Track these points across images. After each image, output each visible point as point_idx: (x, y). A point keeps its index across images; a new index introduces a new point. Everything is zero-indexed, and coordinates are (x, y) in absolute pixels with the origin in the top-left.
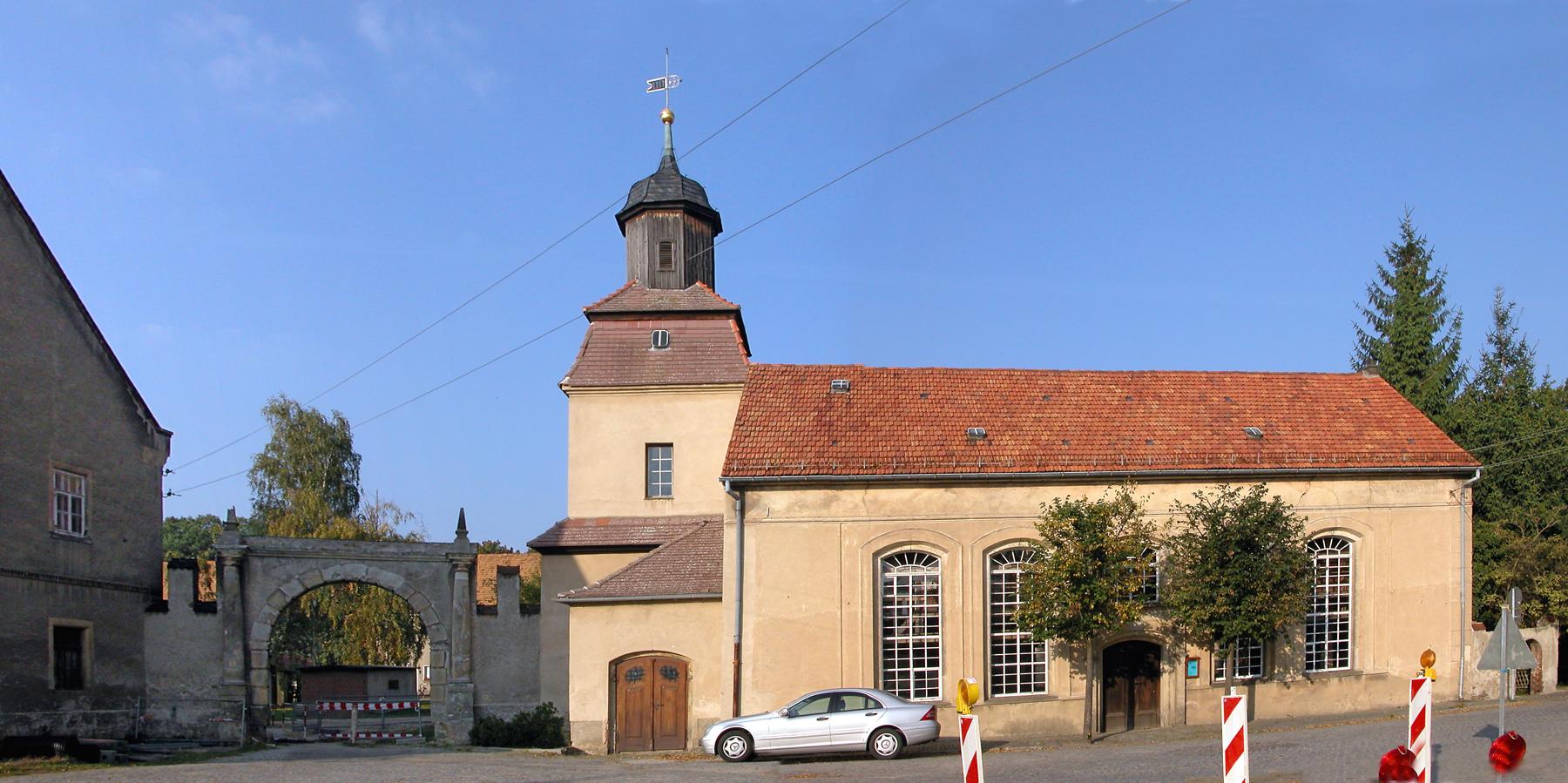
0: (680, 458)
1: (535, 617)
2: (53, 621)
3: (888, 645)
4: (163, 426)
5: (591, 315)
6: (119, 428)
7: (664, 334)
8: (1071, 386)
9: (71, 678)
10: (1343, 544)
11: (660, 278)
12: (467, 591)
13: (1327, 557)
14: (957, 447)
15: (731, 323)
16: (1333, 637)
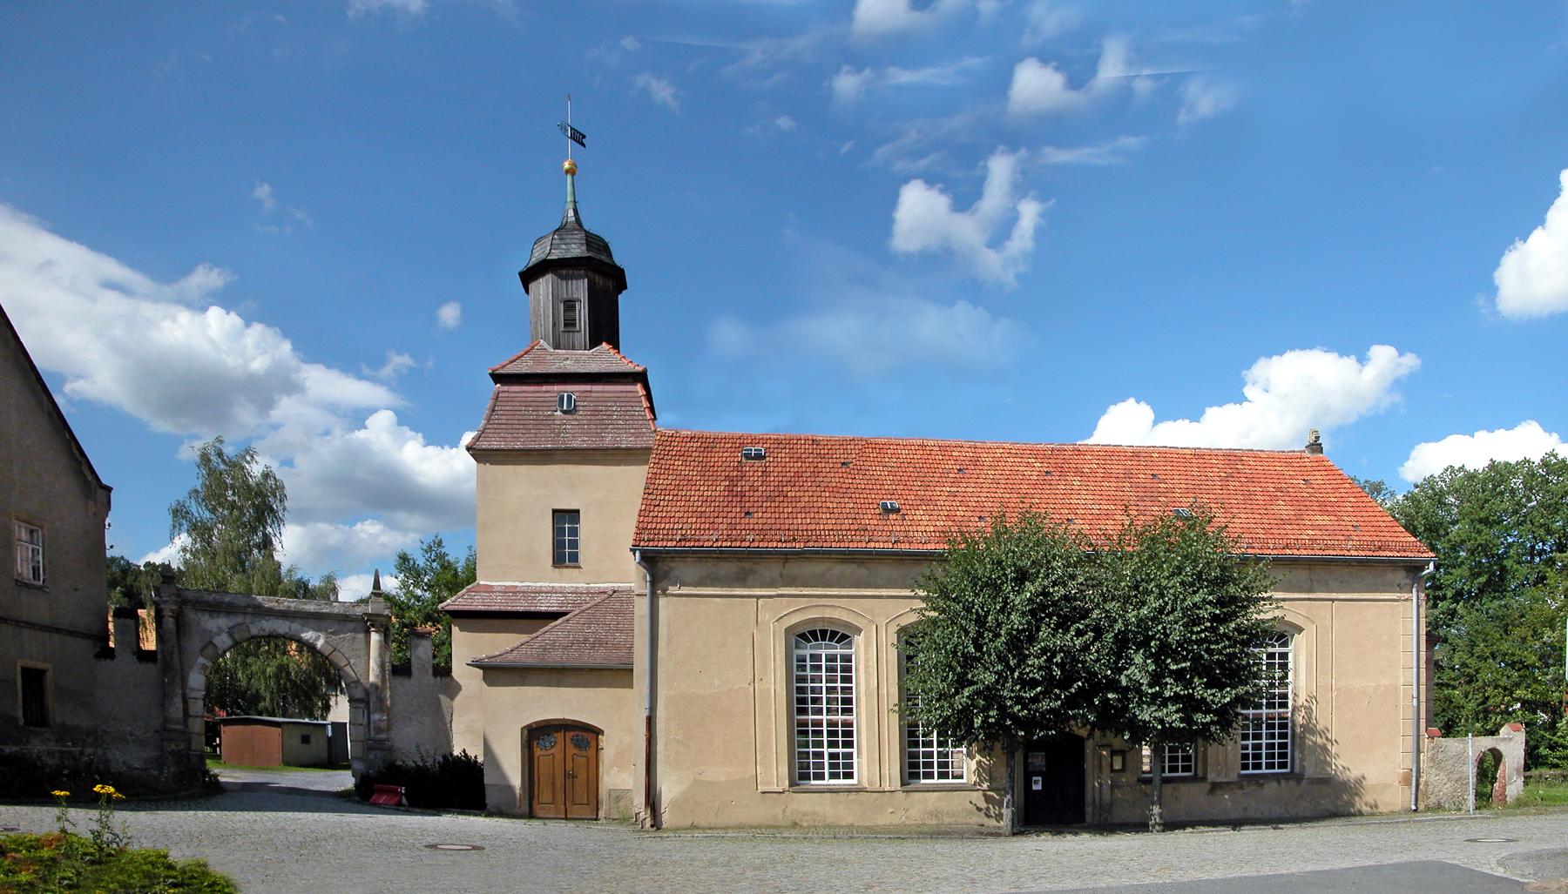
0: (585, 526)
2: (20, 663)
4: (104, 482)
5: (497, 378)
6: (65, 483)
7: (569, 398)
8: (987, 459)
9: (37, 716)
11: (563, 338)
14: (871, 521)
15: (639, 387)
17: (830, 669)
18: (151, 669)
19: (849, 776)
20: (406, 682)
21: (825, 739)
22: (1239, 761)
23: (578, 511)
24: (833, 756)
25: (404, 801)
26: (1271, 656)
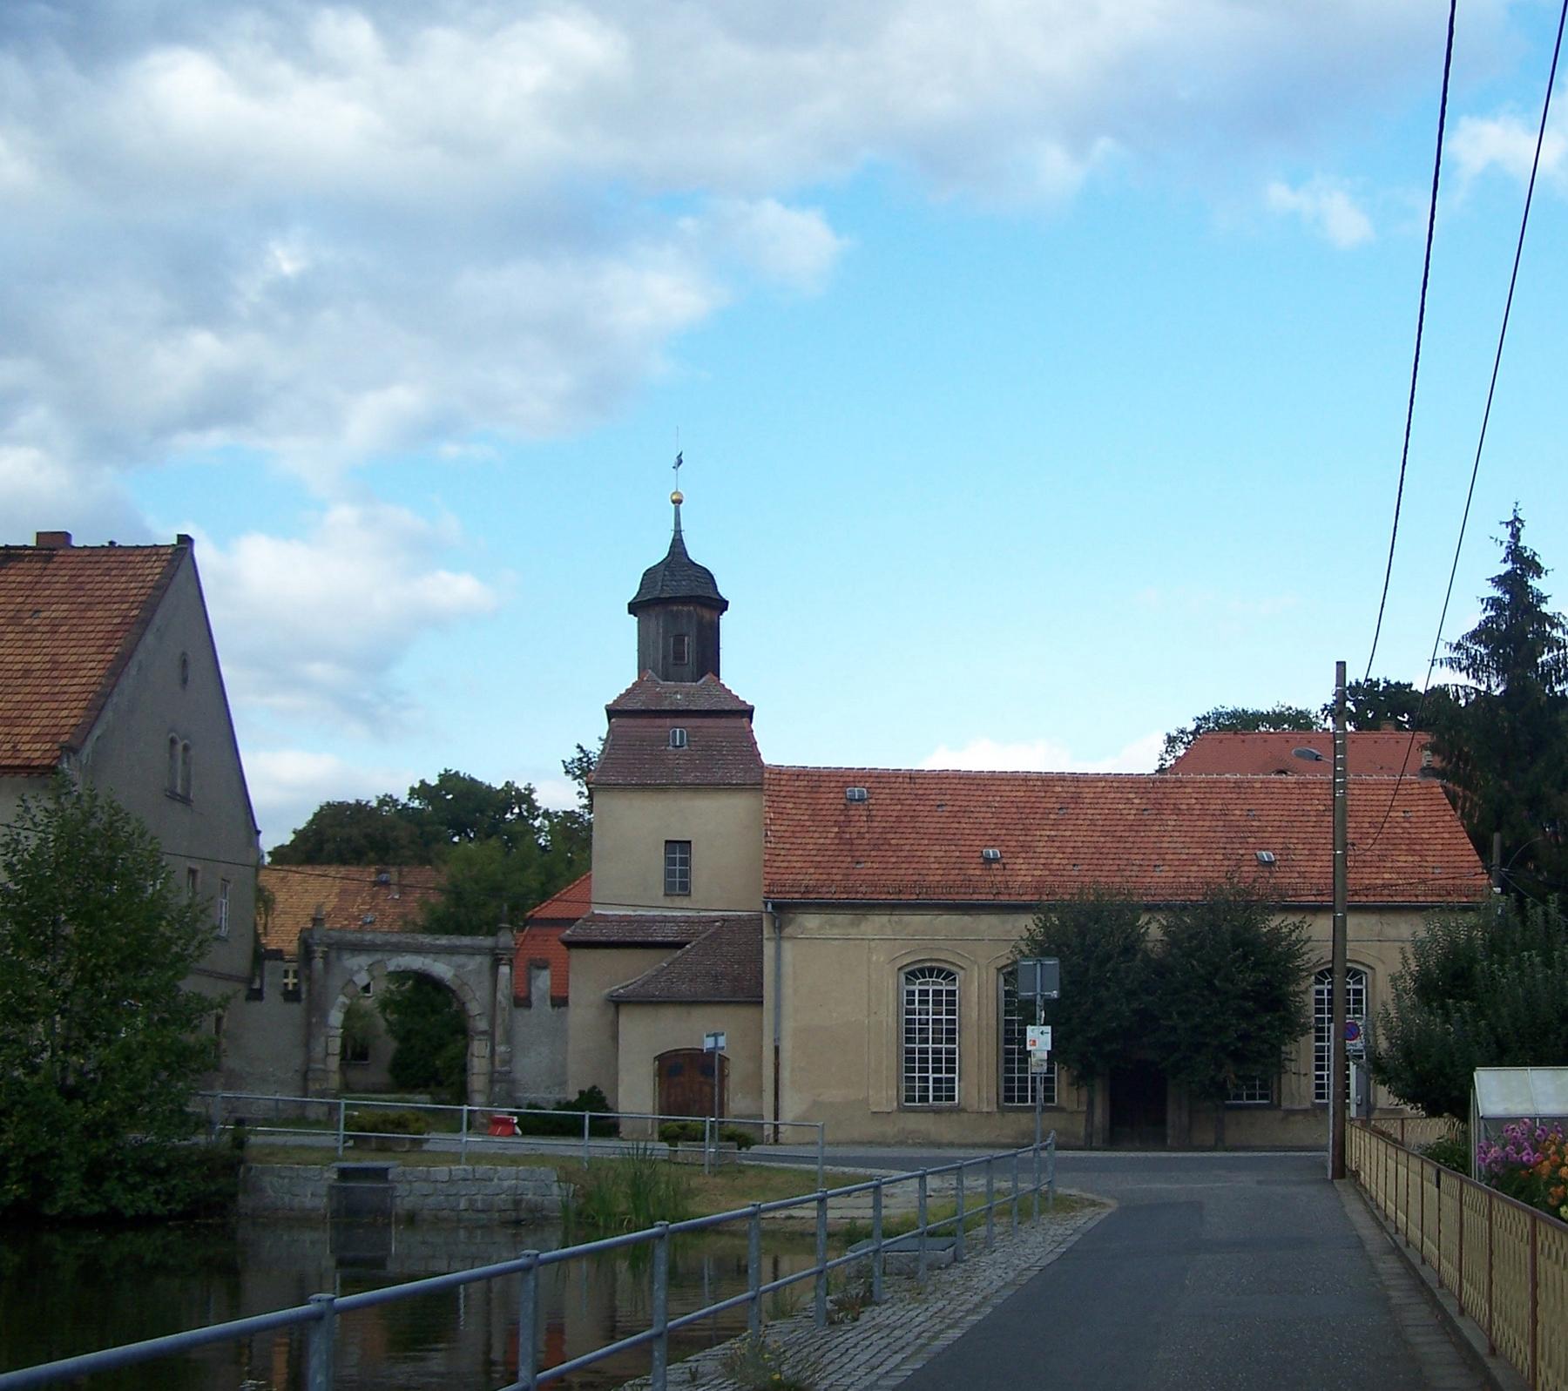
0: (698, 855)
3: (910, 1051)
8: (1088, 794)
10: (949, 976)
17: (937, 1003)
18: (296, 1009)
20: (526, 1012)
25: (518, 1130)
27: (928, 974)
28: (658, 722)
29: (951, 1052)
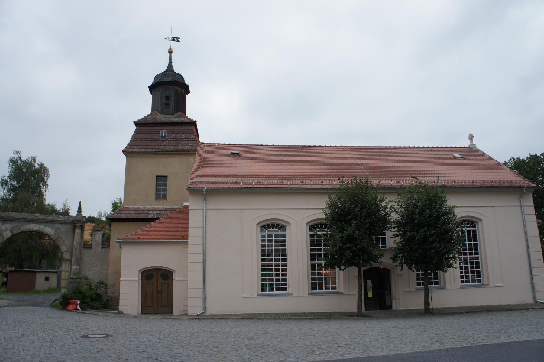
0: (171, 183)
1: (108, 249)
10: (282, 227)
12: (80, 236)
13: (273, 234)
16: (472, 267)
17: (276, 241)
19: (285, 289)
20: (89, 251)
21: (274, 272)
22: (460, 279)
23: (167, 176)
24: (277, 280)
25: (79, 307)
26: (469, 232)
27: (273, 227)
28: (156, 128)
29: (477, 258)
